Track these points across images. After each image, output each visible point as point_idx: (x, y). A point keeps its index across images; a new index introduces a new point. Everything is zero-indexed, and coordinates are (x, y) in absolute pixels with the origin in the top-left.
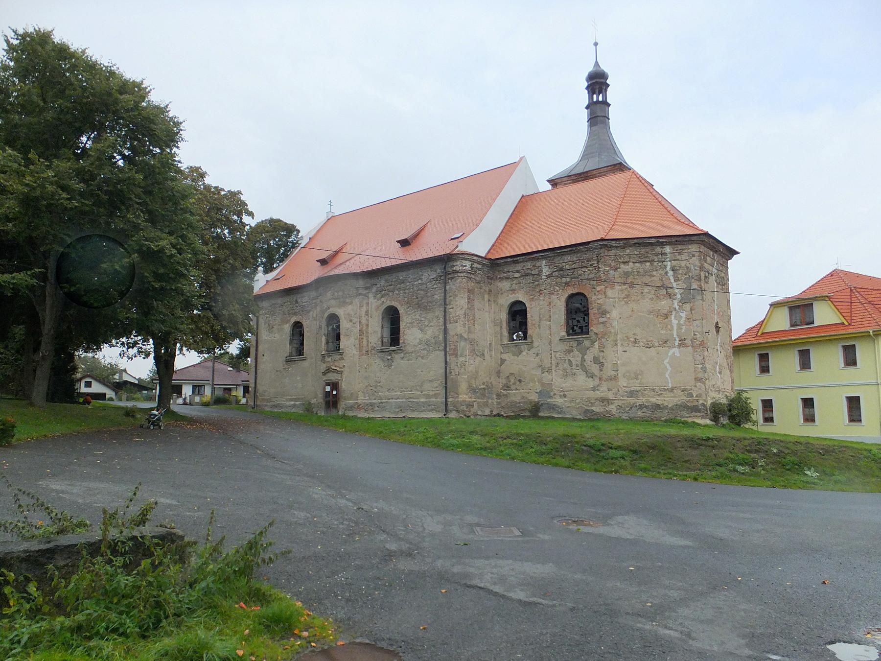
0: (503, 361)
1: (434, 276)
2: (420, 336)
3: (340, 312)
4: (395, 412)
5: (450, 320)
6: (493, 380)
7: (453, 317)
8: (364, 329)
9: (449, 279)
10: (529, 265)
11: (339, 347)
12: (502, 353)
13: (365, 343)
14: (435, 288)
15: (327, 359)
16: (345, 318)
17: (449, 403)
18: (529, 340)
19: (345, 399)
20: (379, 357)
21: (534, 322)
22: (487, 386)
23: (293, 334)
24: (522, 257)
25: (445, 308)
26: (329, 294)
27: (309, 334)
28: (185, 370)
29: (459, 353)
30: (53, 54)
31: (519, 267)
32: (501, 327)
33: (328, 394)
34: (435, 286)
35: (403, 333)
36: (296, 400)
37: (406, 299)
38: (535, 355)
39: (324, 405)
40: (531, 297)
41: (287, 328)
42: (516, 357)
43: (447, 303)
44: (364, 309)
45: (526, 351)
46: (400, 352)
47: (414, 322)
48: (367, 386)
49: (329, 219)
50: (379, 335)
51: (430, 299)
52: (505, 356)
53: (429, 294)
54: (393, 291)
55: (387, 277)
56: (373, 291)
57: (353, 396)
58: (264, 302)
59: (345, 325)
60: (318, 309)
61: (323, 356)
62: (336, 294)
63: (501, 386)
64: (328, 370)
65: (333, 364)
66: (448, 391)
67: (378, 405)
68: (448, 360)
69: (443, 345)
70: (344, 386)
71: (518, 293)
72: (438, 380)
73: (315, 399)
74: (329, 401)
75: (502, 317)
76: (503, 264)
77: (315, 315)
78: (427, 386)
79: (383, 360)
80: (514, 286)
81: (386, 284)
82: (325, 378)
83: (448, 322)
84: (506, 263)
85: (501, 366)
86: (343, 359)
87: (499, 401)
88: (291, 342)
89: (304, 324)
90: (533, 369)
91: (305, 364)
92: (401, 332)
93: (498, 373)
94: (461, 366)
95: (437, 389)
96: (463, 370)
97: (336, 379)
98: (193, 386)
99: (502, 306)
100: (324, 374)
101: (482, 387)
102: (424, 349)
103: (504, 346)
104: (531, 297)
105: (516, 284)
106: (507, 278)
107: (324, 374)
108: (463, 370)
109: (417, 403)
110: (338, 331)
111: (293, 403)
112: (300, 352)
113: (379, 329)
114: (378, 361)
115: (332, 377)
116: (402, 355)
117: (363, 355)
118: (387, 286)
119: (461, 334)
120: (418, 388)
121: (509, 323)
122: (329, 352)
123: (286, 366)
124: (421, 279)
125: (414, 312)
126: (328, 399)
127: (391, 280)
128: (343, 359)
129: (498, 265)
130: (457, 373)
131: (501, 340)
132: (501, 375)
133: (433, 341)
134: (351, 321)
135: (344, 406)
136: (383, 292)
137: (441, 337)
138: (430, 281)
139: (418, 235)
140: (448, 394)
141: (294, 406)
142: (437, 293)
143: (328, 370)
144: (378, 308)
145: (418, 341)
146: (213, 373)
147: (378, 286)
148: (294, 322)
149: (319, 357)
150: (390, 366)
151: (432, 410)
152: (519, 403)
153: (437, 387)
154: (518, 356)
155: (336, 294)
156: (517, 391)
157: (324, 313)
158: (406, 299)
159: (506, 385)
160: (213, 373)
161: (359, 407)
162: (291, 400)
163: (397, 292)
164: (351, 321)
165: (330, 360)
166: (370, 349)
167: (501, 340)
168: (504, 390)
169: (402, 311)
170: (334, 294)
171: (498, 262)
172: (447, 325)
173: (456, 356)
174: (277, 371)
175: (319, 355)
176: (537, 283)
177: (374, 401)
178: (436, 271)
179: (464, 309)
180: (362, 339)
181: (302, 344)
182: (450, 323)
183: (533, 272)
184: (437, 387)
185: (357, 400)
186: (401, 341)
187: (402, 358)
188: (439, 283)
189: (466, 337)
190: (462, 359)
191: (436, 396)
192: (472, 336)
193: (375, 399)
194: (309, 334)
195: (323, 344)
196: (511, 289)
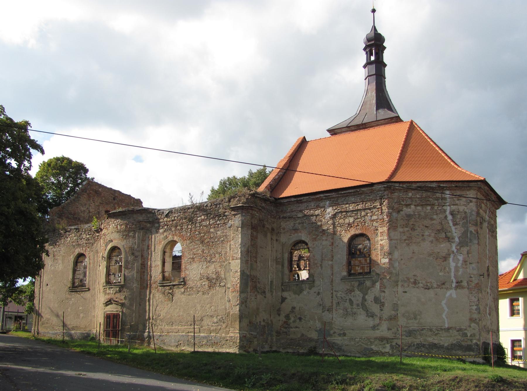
21: (316, 262)
24: (305, 198)
32: (283, 266)
38: (316, 294)
45: (308, 290)
71: (300, 232)
104: (314, 237)
105: (299, 223)
132: (282, 312)
154: (299, 295)
196: (294, 228)
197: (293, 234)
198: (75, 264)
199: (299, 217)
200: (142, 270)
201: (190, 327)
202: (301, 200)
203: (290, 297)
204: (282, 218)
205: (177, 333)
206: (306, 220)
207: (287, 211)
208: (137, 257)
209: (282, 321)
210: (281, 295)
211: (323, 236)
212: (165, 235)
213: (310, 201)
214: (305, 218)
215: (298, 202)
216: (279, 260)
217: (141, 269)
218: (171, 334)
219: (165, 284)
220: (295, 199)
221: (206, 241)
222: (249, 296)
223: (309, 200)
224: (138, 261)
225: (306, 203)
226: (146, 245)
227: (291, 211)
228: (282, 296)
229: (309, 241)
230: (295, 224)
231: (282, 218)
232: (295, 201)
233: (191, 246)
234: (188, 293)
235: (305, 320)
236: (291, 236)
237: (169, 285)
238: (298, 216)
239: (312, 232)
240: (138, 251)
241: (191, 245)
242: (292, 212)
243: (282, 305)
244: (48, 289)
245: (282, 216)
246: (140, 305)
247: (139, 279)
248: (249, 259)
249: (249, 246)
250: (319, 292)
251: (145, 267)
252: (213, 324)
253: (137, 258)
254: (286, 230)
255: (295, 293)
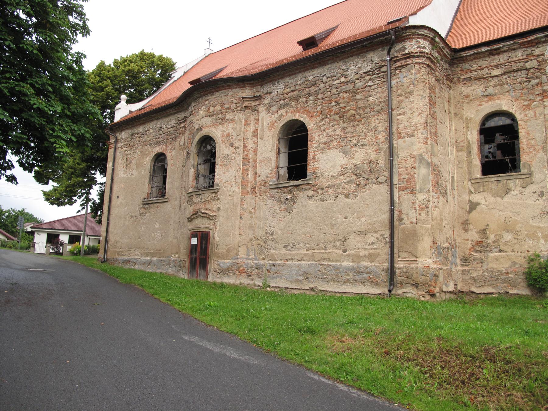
0: (473, 206)
1: (368, 68)
2: (344, 162)
3: (217, 133)
4: (297, 281)
5: (399, 133)
6: (459, 236)
7: (405, 128)
8: (250, 156)
9: (396, 69)
10: (519, 54)
11: (213, 183)
12: (471, 192)
13: (250, 177)
14: (370, 86)
15: (195, 199)
16: (224, 142)
17: (398, 271)
18: (524, 170)
19: (218, 257)
20: (273, 197)
21: (533, 142)
22: (450, 244)
23: (154, 170)
24: (507, 43)
25: (390, 116)
26: (202, 112)
27: (172, 162)
28: (67, 219)
29: (418, 187)
30: (80, 89)
31: (502, 58)
32: (469, 153)
33: (193, 248)
34: (370, 83)
35: (314, 158)
36: (152, 255)
37: (319, 108)
38: (536, 195)
39: (187, 264)
40: (526, 103)
41: (148, 161)
42: (499, 199)
43: (393, 107)
44: (251, 128)
45: (519, 188)
46: (307, 187)
47: (332, 141)
48: (251, 240)
49: (206, 56)
50: (274, 164)
51: (361, 104)
52: (476, 198)
53: (358, 97)
54: (297, 99)
55: (288, 80)
56: (266, 102)
57: (228, 253)
58: (123, 133)
59: (222, 150)
60: (187, 133)
61: (190, 196)
62: (212, 109)
63: (469, 245)
64: (196, 215)
65: (204, 207)
66: (396, 251)
67: (268, 267)
68: (396, 198)
69: (387, 173)
70: (217, 239)
71: (499, 98)
72: (376, 232)
73: (177, 255)
74: (196, 258)
75: (469, 137)
76: (471, 58)
77: (182, 143)
78: (354, 242)
79: (279, 201)
80: (491, 90)
81: (285, 91)
82: (190, 226)
83: (395, 136)
84: (476, 57)
85: (470, 212)
86: (218, 199)
87: (466, 268)
88: (151, 180)
89: (168, 155)
90: (533, 217)
91: (167, 207)
92: (310, 156)
93: (465, 225)
94: (421, 209)
95: (375, 246)
96: (423, 214)
97: (207, 228)
98: (70, 236)
99: (468, 121)
100: (190, 219)
101: (446, 245)
102: (349, 182)
103: (474, 182)
104: (526, 103)
105: (495, 86)
106: (477, 79)
107: (190, 219)
108: (423, 214)
109: (337, 269)
110: (213, 161)
111: (149, 258)
112: (162, 193)
113: (273, 155)
114: (270, 202)
115: (201, 224)
116: (311, 192)
117: (247, 194)
118: (287, 93)
119: (421, 155)
120: (338, 244)
121: (481, 145)
122: (198, 191)
123: (143, 211)
124: (346, 76)
125: (332, 126)
126: (194, 256)
127: (294, 84)
128: (218, 199)
129: (463, 60)
130: (414, 220)
131: (470, 173)
132: (471, 227)
133: (367, 168)
134: (232, 145)
135: (216, 266)
136: (282, 102)
137: (382, 162)
138: (361, 78)
139: (327, 37)
140: (396, 255)
141: (150, 263)
142: (374, 93)
143: (196, 215)
144: (273, 125)
145: (339, 169)
146: (86, 224)
147: (274, 94)
148: (156, 155)
149: (185, 197)
150: (289, 211)
151: (363, 282)
152: (507, 273)
153: (373, 243)
154: (502, 198)
155: (212, 109)
156: (502, 253)
157: (193, 137)
158: (319, 108)
159: (479, 243)
160: (86, 224)
161: (239, 271)
162: (147, 254)
163: (304, 100)
164: (232, 145)
165: (199, 200)
166: (258, 184)
167: (470, 173)
168: (476, 251)
169: (311, 125)
170: (209, 110)
171: (464, 54)
172: (394, 142)
173: (413, 191)
174: (132, 217)
175: (184, 194)
176: (537, 81)
177: (262, 262)
178: (371, 61)
179: (424, 115)
180: (247, 170)
181: (164, 183)
182: (400, 137)
183: (528, 65)
184: (373, 243)
185: (237, 259)
186: (310, 168)
187: (311, 198)
188: (379, 77)
189: (429, 160)
190: (421, 197)
191: (371, 257)
192: (436, 161)
193: (264, 259)
194: (172, 162)
195: (191, 179)
196: (486, 94)
197: (486, 103)
198: (152, 168)
199: (493, 77)
200: (244, 167)
201: (323, 251)
202: (500, 48)
203: (486, 201)
204: (463, 81)
205: (300, 260)
206: (508, 79)
207: (472, 69)
208: (238, 148)
209: (472, 241)
210: (468, 199)
211: (544, 100)
212: (279, 114)
213: (514, 49)
214: (506, 76)
215: (492, 53)
216: (462, 144)
217: (243, 166)
218: (290, 262)
219: (280, 186)
220: (489, 48)
221: (349, 114)
222: (431, 197)
223: (513, 47)
224: (239, 154)
225: (507, 53)
226: (251, 131)
227: (479, 68)
228: (470, 201)
229: (516, 111)
230: (487, 87)
231: (463, 81)
232: (487, 51)
233: (323, 124)
234: (319, 197)
235: (517, 239)
236: (482, 107)
237: (288, 187)
238: (492, 75)
239: (521, 96)
240: (239, 140)
241: (323, 122)
242: (482, 69)
243: (471, 214)
244: (118, 203)
245: (462, 77)
246: (241, 218)
247: (241, 180)
248: (429, 136)
249: (427, 116)
250: (542, 192)
251: (249, 162)
252: (367, 247)
253: (238, 151)
254: (471, 98)
255: (496, 195)
